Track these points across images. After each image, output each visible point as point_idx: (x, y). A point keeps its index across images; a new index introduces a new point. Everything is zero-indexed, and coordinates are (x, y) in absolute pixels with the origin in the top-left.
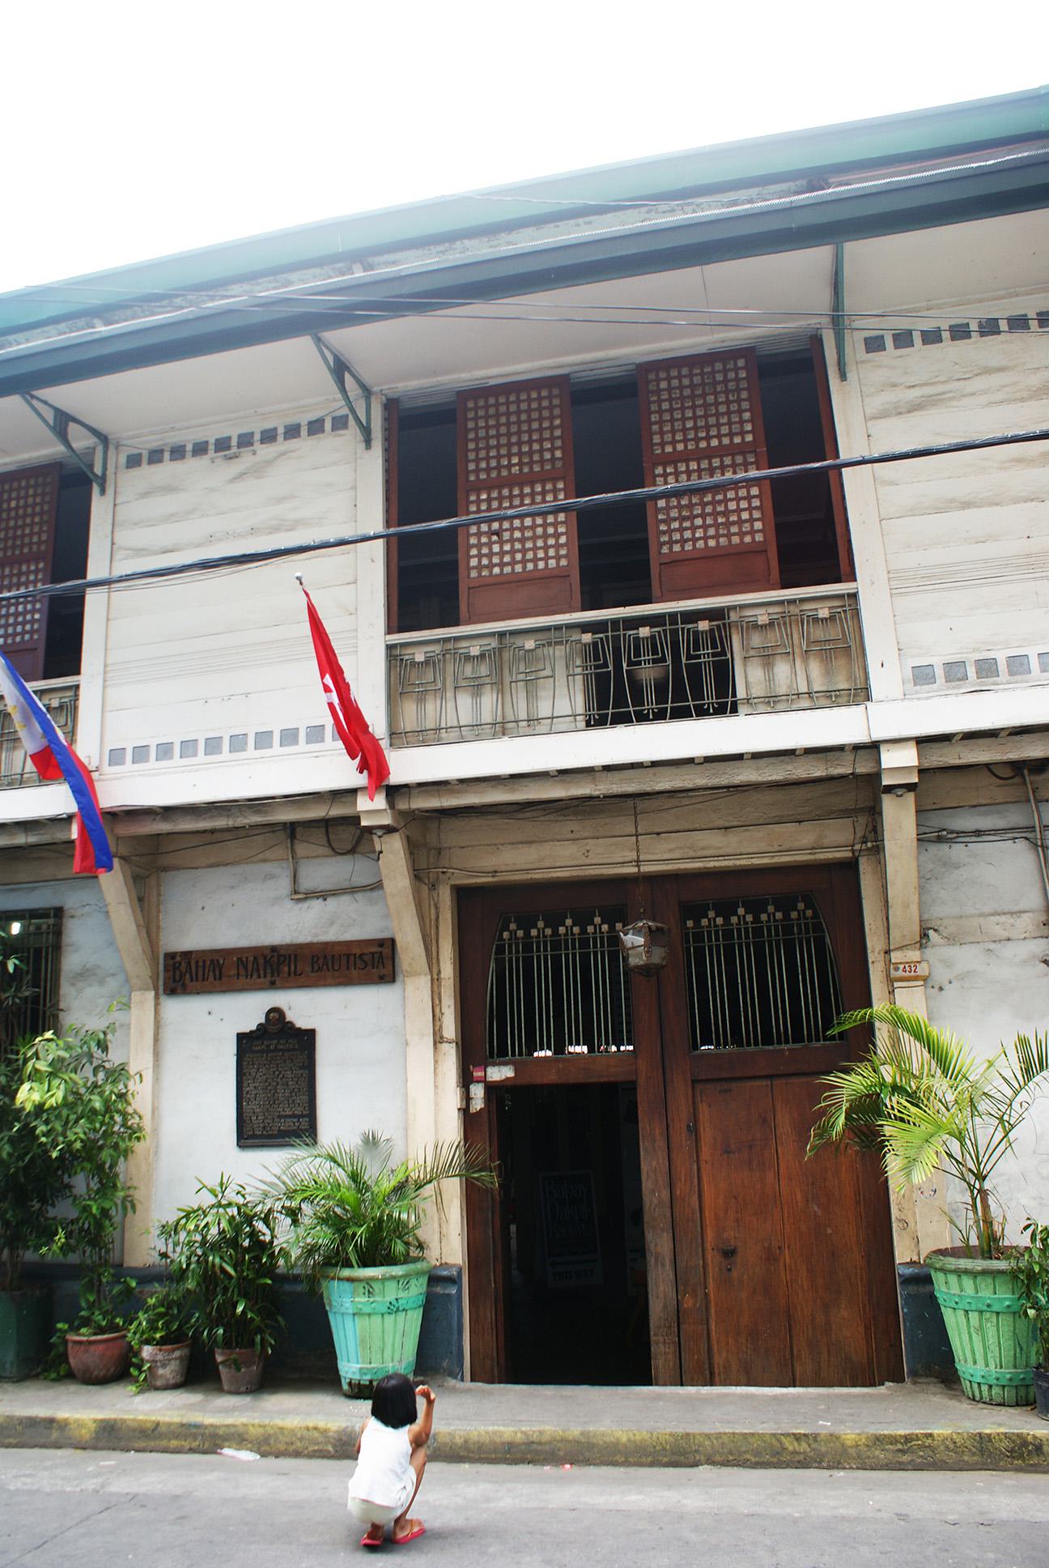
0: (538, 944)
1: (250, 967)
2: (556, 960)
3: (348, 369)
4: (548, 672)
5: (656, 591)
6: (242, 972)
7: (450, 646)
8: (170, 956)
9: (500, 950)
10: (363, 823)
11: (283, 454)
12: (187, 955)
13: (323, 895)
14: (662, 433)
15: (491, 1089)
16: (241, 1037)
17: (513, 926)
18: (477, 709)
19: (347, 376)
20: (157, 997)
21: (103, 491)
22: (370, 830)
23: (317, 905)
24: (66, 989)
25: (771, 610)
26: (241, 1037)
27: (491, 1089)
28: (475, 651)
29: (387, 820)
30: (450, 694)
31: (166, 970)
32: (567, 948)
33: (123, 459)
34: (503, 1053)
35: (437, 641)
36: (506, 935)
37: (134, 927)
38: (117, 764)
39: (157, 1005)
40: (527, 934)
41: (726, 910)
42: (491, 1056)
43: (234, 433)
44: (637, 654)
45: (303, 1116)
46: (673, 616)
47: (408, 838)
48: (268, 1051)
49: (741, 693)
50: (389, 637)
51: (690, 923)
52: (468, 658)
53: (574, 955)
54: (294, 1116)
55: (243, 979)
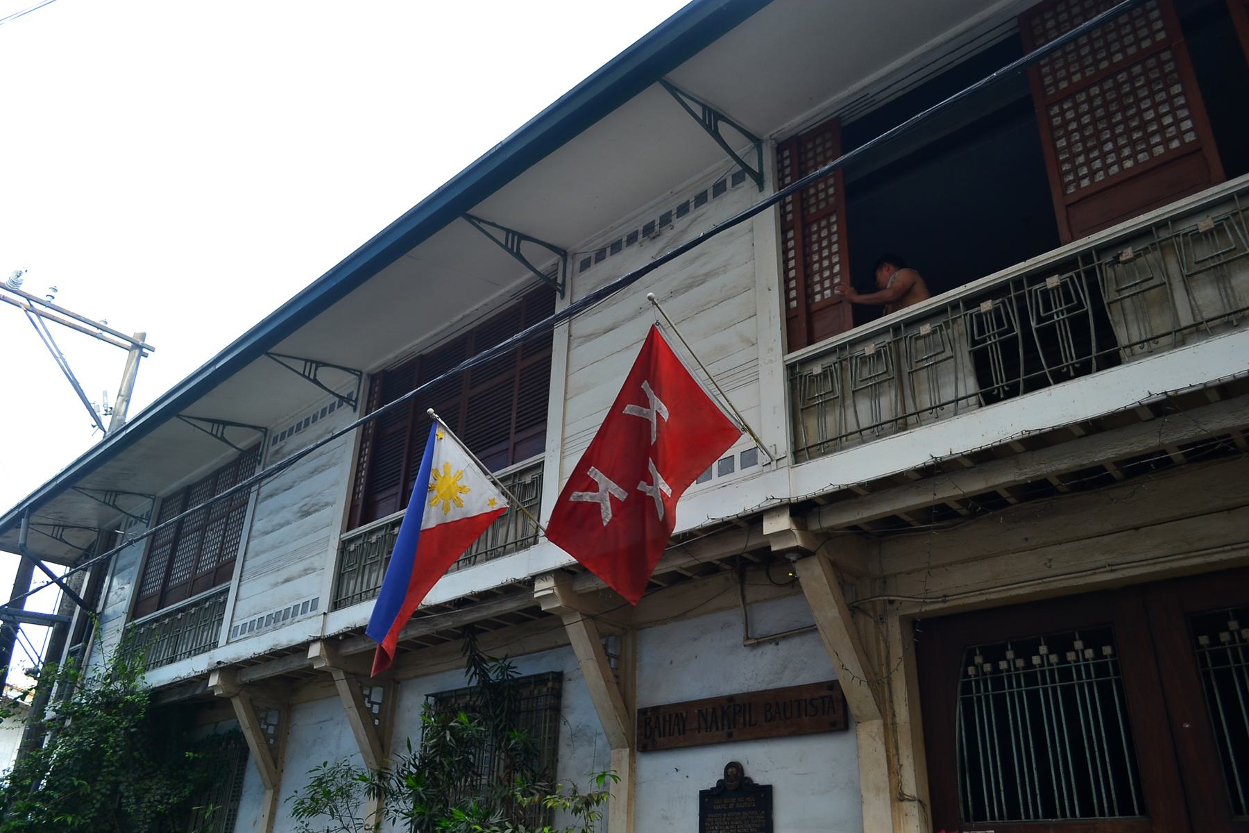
0: (1010, 678)
2: (1033, 696)
3: (720, 117)
4: (948, 353)
5: (1063, 230)
7: (846, 354)
8: (643, 712)
9: (967, 688)
10: (773, 549)
11: (693, 221)
12: (656, 709)
13: (775, 639)
14: (1054, 72)
16: (704, 795)
17: (978, 660)
18: (876, 411)
19: (723, 127)
20: (632, 755)
21: (563, 296)
23: (770, 649)
24: (564, 750)
26: (704, 795)
29: (797, 542)
30: (849, 402)
31: (639, 727)
32: (1044, 682)
33: (578, 266)
36: (971, 670)
37: (603, 683)
40: (996, 668)
42: (968, 820)
43: (656, 217)
44: (1048, 307)
47: (833, 564)
51: (1204, 640)
52: (864, 359)
53: (1054, 689)
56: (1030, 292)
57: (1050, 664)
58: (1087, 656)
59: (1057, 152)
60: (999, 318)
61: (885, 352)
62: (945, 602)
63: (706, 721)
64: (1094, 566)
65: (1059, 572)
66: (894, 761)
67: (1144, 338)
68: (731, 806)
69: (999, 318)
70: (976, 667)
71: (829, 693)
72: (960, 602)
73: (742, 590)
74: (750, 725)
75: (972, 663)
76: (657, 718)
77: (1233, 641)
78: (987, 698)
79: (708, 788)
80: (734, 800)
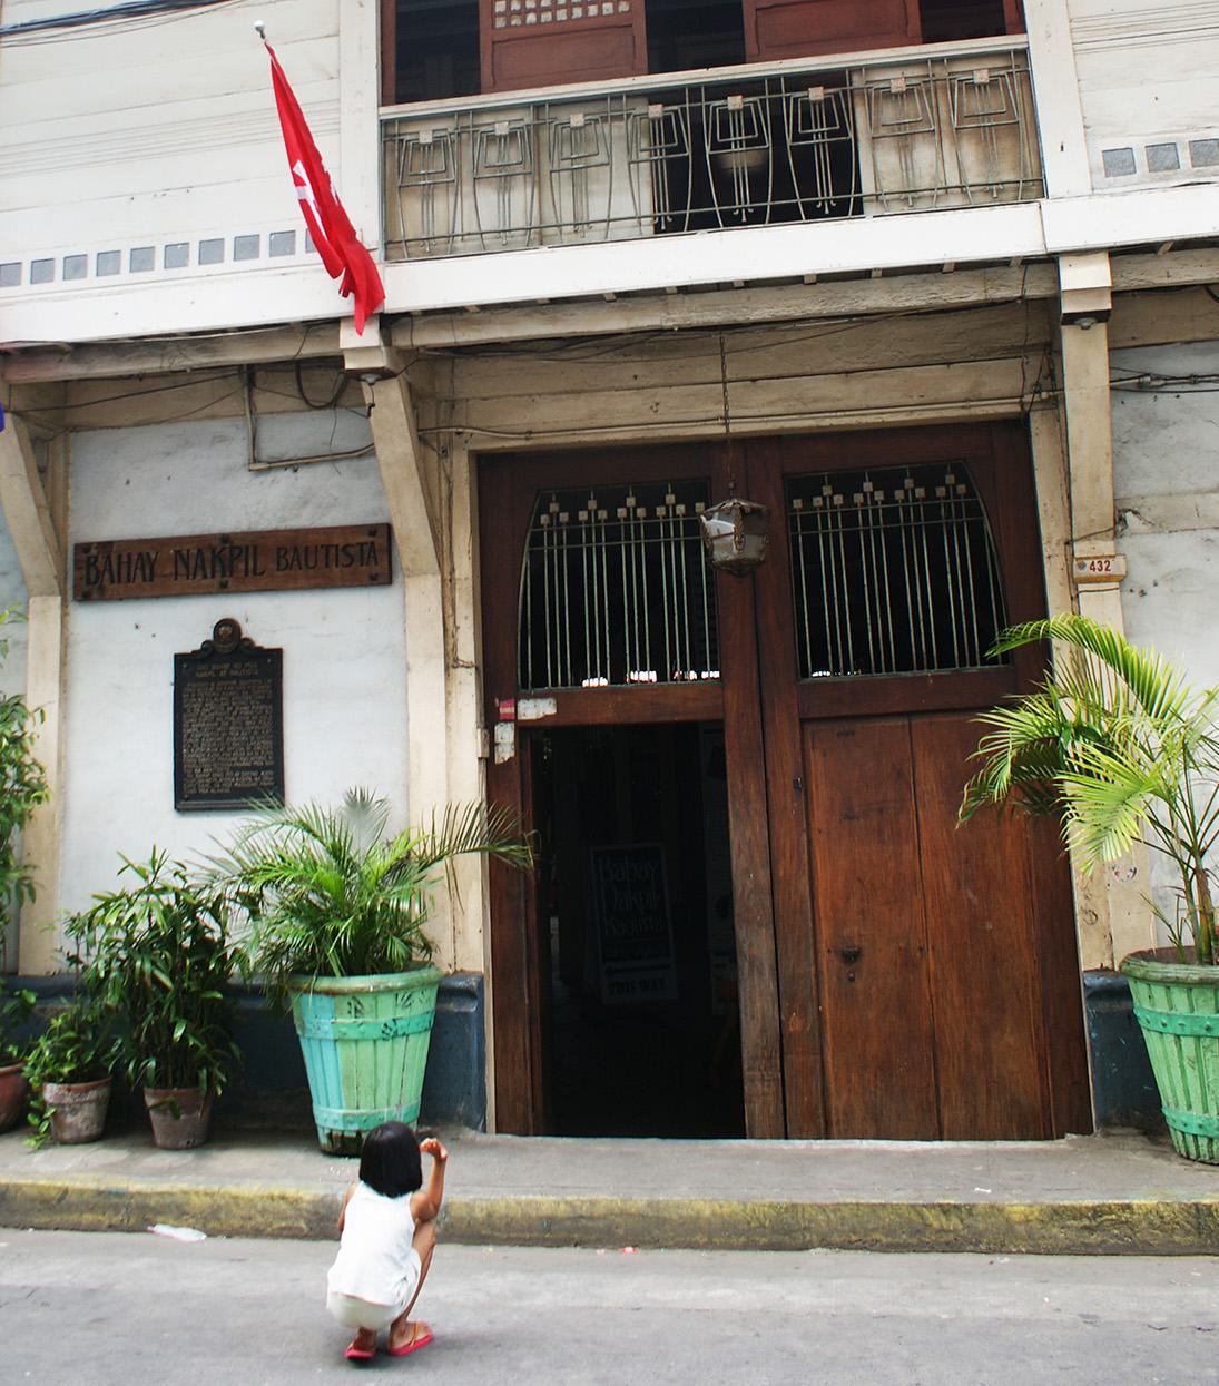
1: (192, 563)
2: (614, 554)
4: (602, 158)
6: (182, 570)
8: (83, 548)
9: (537, 540)
12: (106, 546)
13: (293, 464)
15: (524, 731)
16: (180, 660)
17: (554, 507)
18: (505, 209)
20: (64, 605)
22: (357, 375)
23: (284, 477)
25: (909, 72)
26: (180, 660)
27: (524, 731)
28: (502, 129)
29: (380, 361)
30: (467, 188)
31: (77, 567)
32: (628, 538)
34: (540, 681)
35: (450, 115)
36: (544, 519)
38: (139, 270)
39: (64, 615)
41: (847, 484)
44: (725, 134)
45: (265, 768)
46: (774, 81)
48: (217, 679)
49: (868, 187)
50: (384, 110)
51: (797, 503)
52: (492, 138)
54: (253, 768)
55: (182, 580)
56: (788, 99)
57: (636, 518)
58: (678, 512)
59: (493, 15)
60: (748, 121)
61: (522, 136)
62: (527, 439)
63: (187, 567)
64: (704, 417)
65: (666, 418)
66: (450, 622)
67: (501, 228)
68: (222, 674)
69: (748, 121)
70: (551, 515)
71: (371, 539)
72: (547, 441)
73: (250, 396)
74: (255, 573)
75: (546, 511)
76: (109, 557)
77: (865, 504)
78: (836, 536)
79: (188, 649)
80: (227, 666)
